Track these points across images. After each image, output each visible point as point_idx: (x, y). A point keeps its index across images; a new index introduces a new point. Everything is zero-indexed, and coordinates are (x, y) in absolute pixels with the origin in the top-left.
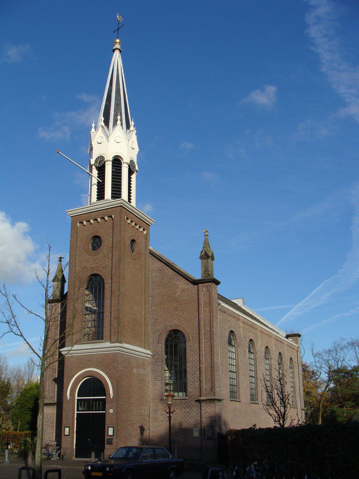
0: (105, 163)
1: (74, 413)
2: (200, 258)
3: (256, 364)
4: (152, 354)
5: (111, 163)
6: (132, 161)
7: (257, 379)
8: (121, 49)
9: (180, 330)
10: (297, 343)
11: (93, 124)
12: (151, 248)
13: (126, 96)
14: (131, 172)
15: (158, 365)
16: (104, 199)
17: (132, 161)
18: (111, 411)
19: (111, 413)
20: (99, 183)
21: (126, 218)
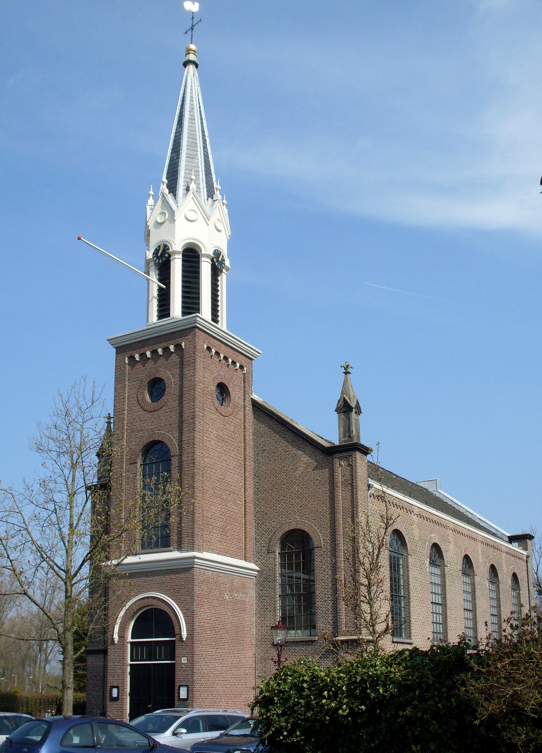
0: (170, 256)
1: (124, 664)
2: (336, 411)
3: (445, 583)
4: (258, 569)
5: (180, 256)
6: (217, 254)
7: (446, 606)
8: (197, 62)
9: (305, 530)
10: (526, 549)
11: (150, 191)
12: (255, 397)
13: (208, 142)
14: (216, 272)
15: (269, 587)
16: (169, 316)
17: (217, 254)
18: (184, 660)
19: (184, 664)
20: (160, 289)
21: (205, 347)
